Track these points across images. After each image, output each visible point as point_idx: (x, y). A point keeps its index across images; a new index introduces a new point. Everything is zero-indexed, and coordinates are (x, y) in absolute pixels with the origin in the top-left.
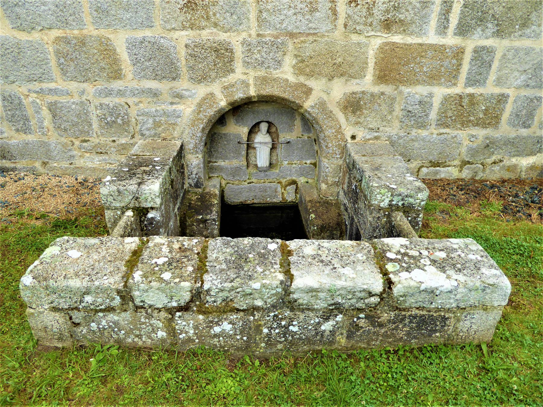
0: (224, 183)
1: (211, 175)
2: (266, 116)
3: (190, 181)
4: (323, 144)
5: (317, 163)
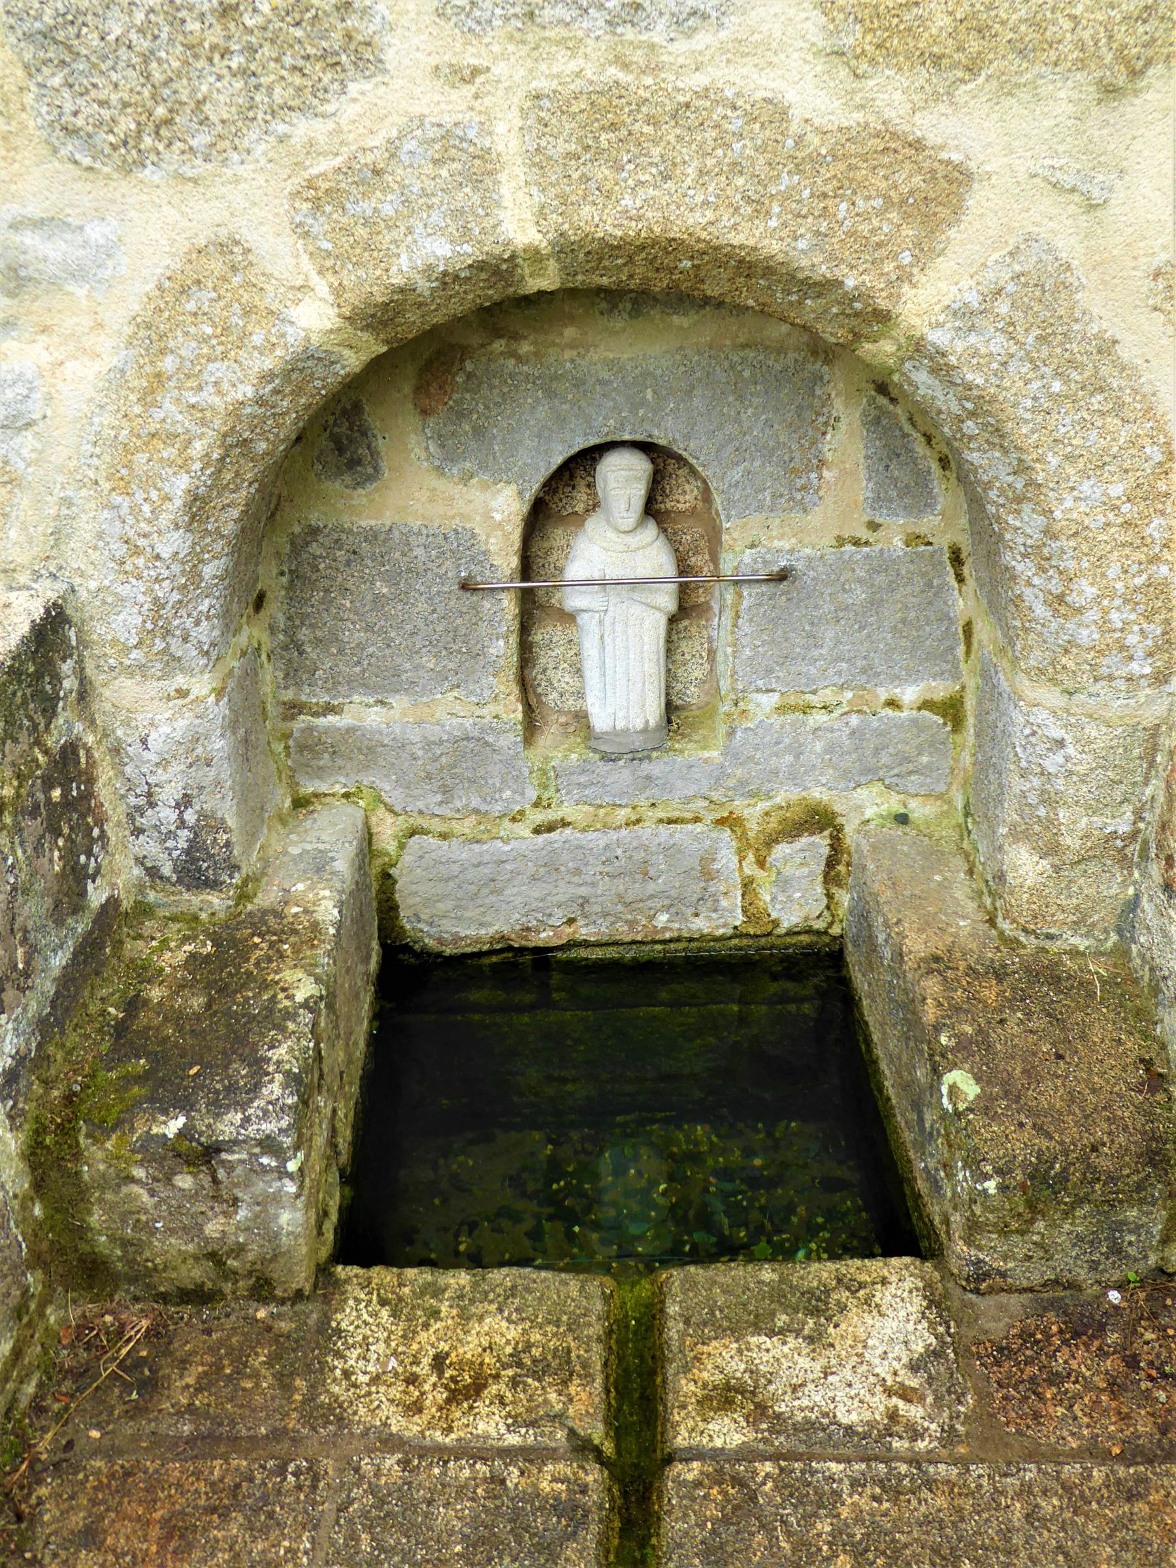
0: (387, 831)
1: (309, 787)
2: (634, 409)
3: (149, 846)
4: (1032, 586)
5: (970, 703)
